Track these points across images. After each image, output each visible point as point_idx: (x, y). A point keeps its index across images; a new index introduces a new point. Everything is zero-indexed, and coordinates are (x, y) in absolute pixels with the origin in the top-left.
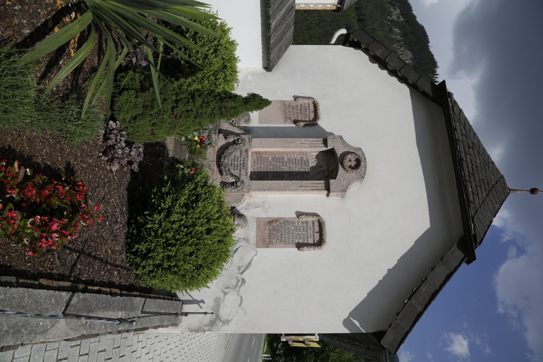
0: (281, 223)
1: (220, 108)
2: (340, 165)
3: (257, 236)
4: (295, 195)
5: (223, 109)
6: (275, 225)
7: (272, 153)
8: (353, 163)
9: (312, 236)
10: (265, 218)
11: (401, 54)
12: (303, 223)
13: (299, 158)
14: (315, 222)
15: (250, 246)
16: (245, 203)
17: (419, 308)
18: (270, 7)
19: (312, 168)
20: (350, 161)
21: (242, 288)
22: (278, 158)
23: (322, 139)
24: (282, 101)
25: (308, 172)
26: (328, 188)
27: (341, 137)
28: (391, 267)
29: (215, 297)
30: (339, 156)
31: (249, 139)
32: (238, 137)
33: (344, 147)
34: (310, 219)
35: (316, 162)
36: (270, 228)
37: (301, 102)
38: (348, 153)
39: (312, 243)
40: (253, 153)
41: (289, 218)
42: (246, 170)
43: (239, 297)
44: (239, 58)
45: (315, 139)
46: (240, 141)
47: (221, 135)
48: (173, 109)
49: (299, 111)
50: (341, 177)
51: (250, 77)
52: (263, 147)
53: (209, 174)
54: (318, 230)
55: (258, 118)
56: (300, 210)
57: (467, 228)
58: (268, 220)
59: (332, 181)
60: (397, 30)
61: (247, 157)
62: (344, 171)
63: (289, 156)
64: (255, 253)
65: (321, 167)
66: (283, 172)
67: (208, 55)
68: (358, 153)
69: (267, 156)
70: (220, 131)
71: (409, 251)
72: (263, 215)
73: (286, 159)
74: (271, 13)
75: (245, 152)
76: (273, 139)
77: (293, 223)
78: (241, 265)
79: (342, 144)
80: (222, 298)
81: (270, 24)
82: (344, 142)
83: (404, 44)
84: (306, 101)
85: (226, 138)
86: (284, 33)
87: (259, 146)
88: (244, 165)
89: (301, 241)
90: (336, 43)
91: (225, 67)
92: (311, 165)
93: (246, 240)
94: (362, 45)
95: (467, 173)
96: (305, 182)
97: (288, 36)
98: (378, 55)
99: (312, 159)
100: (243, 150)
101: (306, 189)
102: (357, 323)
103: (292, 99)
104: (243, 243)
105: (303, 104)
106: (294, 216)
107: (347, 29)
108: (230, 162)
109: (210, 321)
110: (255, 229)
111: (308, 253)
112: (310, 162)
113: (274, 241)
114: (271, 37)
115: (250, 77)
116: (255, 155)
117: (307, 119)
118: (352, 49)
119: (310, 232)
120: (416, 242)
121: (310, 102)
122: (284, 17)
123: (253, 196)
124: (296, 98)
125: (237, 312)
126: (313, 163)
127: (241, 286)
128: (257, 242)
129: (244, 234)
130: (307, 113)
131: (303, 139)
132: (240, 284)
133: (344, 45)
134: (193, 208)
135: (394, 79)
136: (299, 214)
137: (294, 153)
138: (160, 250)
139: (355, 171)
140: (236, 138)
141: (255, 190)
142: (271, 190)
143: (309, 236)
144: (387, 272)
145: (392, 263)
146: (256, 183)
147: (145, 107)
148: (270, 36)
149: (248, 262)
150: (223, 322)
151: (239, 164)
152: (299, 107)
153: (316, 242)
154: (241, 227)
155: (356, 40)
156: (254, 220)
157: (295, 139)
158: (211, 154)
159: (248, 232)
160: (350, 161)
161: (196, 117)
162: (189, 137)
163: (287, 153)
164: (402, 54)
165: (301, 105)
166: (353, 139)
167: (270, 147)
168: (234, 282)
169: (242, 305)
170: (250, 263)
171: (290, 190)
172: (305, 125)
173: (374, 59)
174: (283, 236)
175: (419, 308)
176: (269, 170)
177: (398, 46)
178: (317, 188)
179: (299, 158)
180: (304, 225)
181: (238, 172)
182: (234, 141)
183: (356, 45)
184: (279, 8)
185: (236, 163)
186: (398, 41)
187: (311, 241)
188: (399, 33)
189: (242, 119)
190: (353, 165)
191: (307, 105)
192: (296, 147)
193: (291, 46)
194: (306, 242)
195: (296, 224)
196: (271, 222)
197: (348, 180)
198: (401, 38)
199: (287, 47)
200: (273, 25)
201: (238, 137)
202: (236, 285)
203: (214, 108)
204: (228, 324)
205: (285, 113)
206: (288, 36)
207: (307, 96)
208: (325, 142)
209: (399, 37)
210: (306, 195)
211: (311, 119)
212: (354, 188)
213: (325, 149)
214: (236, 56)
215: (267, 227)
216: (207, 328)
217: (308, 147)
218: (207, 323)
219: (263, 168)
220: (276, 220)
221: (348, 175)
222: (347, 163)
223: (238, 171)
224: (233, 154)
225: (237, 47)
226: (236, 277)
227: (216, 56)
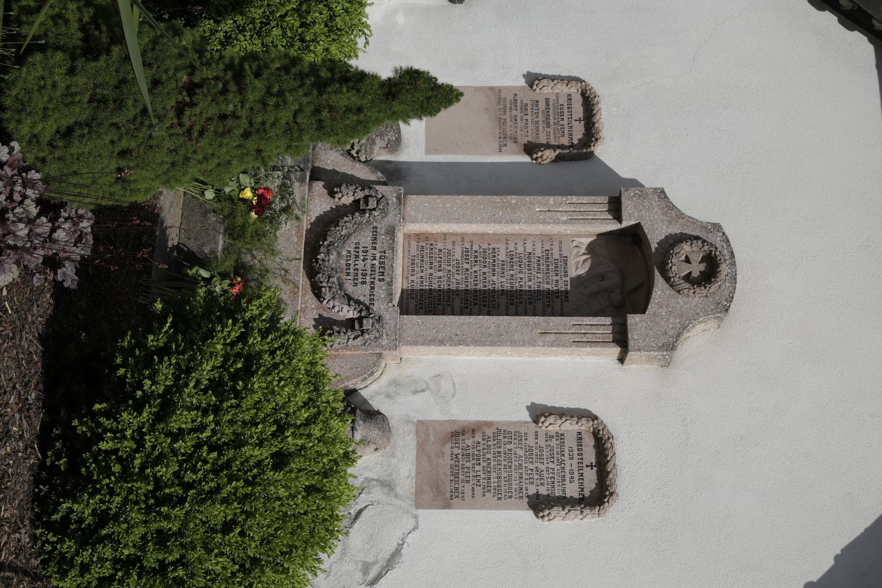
0: (485, 438)
2: (657, 274)
3: (418, 473)
4: (526, 359)
5: (325, 113)
6: (469, 442)
7: (463, 237)
8: (697, 269)
9: (576, 476)
12: (549, 437)
13: (538, 253)
14: (573, 97)
15: (398, 502)
16: (384, 380)
19: (577, 281)
20: (687, 260)
22: (479, 253)
23: (605, 199)
24: (491, 88)
25: (566, 292)
26: (621, 339)
27: (663, 191)
30: (654, 246)
31: (399, 198)
33: (670, 222)
34: (570, 427)
35: (588, 264)
36: (456, 451)
38: (682, 238)
40: (408, 237)
41: (511, 423)
42: (390, 284)
45: (585, 199)
46: (372, 203)
47: (319, 186)
48: (180, 111)
49: (541, 118)
51: (400, 19)
52: (438, 222)
53: (285, 297)
54: (593, 460)
55: (424, 137)
59: (633, 320)
61: (393, 249)
62: (669, 291)
63: (511, 247)
64: (411, 523)
65: (602, 277)
66: (494, 291)
68: (711, 238)
69: (450, 247)
70: (317, 174)
72: (436, 415)
73: (502, 256)
75: (387, 233)
76: (467, 198)
77: (520, 437)
78: (370, 559)
79: (665, 214)
82: (671, 207)
84: (562, 89)
85: (332, 194)
87: (426, 219)
88: (383, 271)
89: (543, 491)
92: (573, 273)
93: (388, 485)
96: (555, 322)
99: (577, 255)
100: (382, 228)
101: (558, 341)
103: (522, 82)
104: (377, 494)
105: (552, 98)
106: (526, 417)
108: (343, 262)
110: (414, 453)
111: (565, 526)
112: (571, 262)
113: (468, 488)
115: (400, 19)
116: (414, 244)
117: (565, 141)
119: (571, 465)
124: (533, 80)
126: (579, 266)
128: (419, 492)
129: (380, 466)
130: (565, 122)
131: (551, 200)
135: (829, 19)
136: (539, 413)
137: (525, 238)
138: (136, 516)
139: (701, 291)
140: (360, 195)
141: (415, 343)
143: (568, 476)
149: (392, 549)
151: (368, 267)
152: (542, 105)
153: (587, 493)
154: (373, 447)
156: (411, 427)
157: (528, 199)
158: (290, 238)
159: (394, 461)
160: (687, 260)
161: (246, 135)
163: (507, 238)
165: (547, 100)
167: (458, 220)
170: (396, 554)
171: (513, 343)
172: (558, 159)
176: (453, 287)
178: (590, 338)
179: (538, 253)
180: (554, 443)
181: (367, 292)
182: (357, 202)
185: (360, 264)
187: (572, 491)
190: (696, 274)
191: (563, 100)
192: (531, 221)
194: (558, 493)
195: (531, 441)
196: (459, 433)
197: (681, 316)
201: (367, 192)
205: (501, 122)
207: (564, 74)
208: (615, 208)
211: (575, 141)
212: (699, 340)
213: (614, 226)
219: (437, 279)
220: (472, 429)
222: (678, 268)
223: (367, 288)
224: (353, 240)
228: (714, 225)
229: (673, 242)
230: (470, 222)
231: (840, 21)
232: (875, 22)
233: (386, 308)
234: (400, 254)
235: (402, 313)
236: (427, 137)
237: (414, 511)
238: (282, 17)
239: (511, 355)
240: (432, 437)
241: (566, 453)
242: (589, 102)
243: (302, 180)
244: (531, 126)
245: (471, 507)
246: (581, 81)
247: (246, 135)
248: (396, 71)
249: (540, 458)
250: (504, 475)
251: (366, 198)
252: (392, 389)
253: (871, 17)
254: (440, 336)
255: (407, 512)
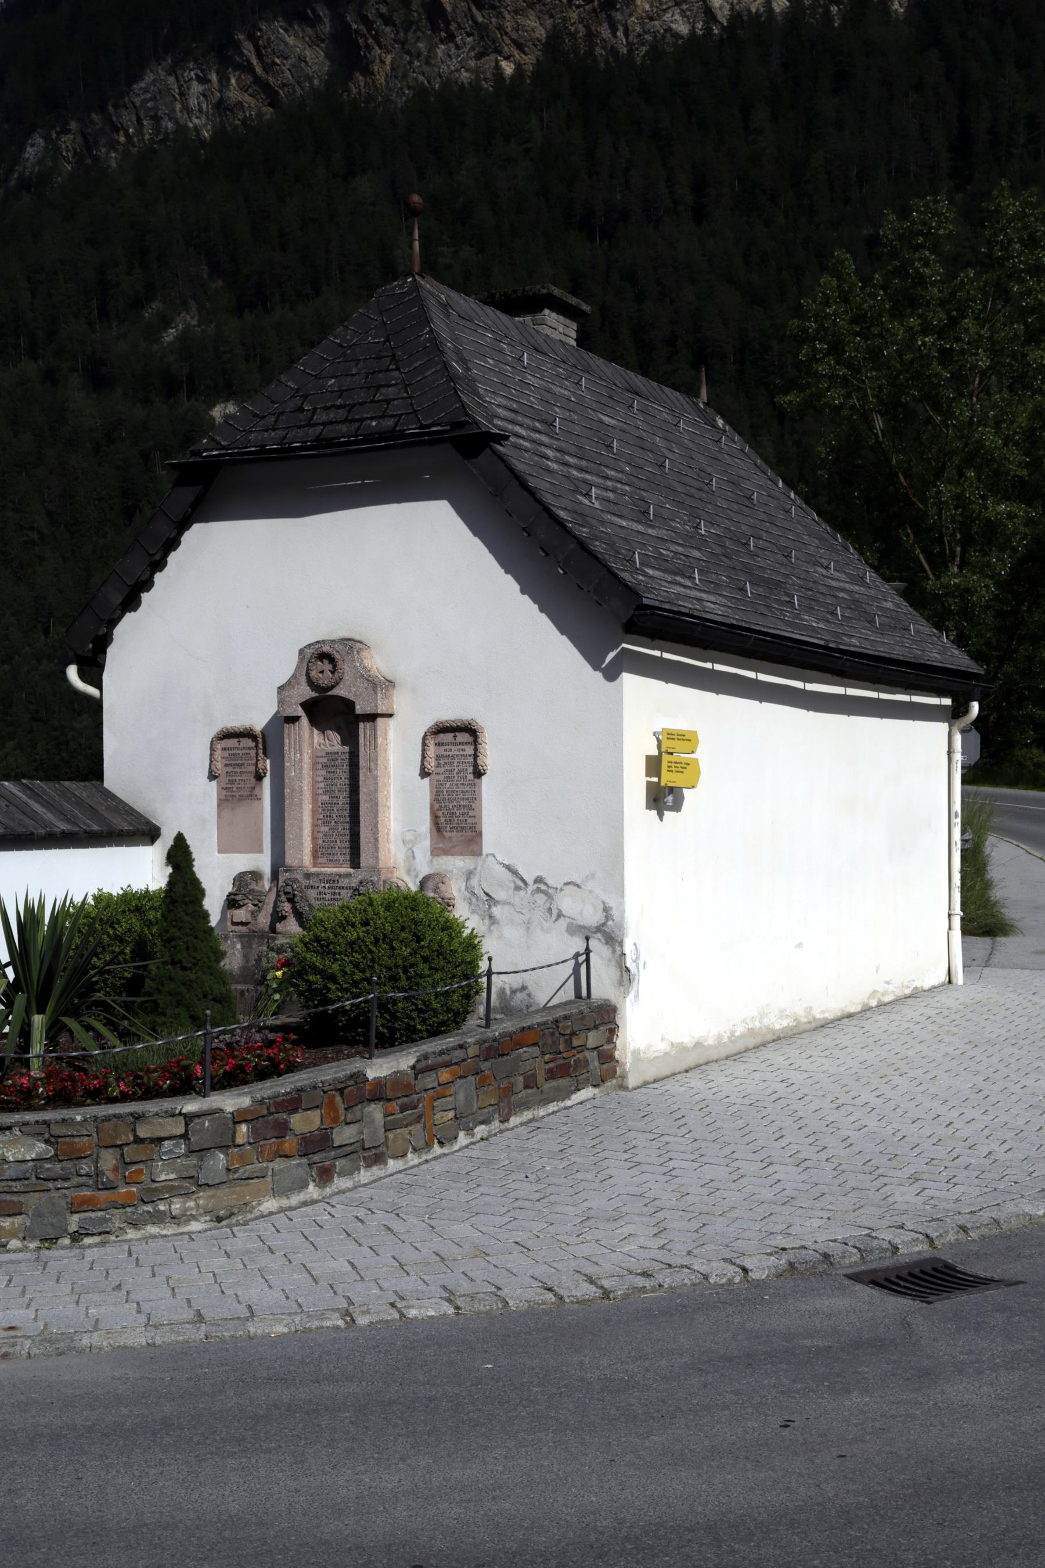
1: (185, 903)
2: (330, 693)
3: (462, 854)
4: (392, 780)
5: (186, 899)
6: (443, 820)
7: (314, 825)
8: (327, 666)
9: (461, 747)
10: (432, 839)
11: (157, 129)
12: (438, 765)
13: (324, 772)
15: (479, 868)
17: (572, 546)
18: (32, 834)
20: (322, 672)
21: (550, 882)
22: (323, 815)
23: (286, 726)
24: (219, 806)
26: (372, 717)
27: (279, 688)
28: (517, 587)
29: (566, 935)
31: (286, 871)
32: (282, 893)
33: (299, 684)
34: (432, 751)
35: (330, 732)
37: (219, 765)
38: (308, 675)
39: (473, 747)
40: (315, 865)
41: (431, 792)
42: (340, 876)
43: (566, 887)
44: (125, 887)
45: (286, 741)
46: (289, 889)
47: (279, 926)
48: (184, 969)
49: (238, 770)
50: (350, 692)
52: (302, 844)
55: (251, 855)
56: (418, 771)
57: (436, 440)
58: (435, 833)
59: (359, 709)
60: (31, 153)
62: (341, 685)
63: (320, 791)
64: (491, 858)
67: (117, 936)
68: (308, 656)
69: (321, 835)
70: (273, 929)
71: (492, 551)
72: (427, 843)
73: (326, 798)
74: (42, 831)
75: (308, 879)
76: (287, 824)
78: (512, 886)
79: (293, 687)
80: (568, 920)
81: (63, 832)
82: (289, 682)
83: (102, 109)
84: (218, 754)
85: (284, 918)
86: (79, 802)
87: (302, 853)
88: (332, 880)
89: (471, 769)
90: (99, 686)
91: (138, 909)
93: (469, 875)
94: (101, 633)
95: (344, 428)
97: (85, 794)
98: (119, 601)
99: (325, 745)
100: (305, 882)
102: (611, 655)
103: (214, 783)
104: (474, 882)
107: (71, 663)
109: (607, 943)
111: (491, 756)
112: (329, 749)
113: (470, 820)
114: (88, 829)
116: (320, 860)
117: (253, 753)
118: (111, 651)
120: (475, 535)
121: (219, 746)
122: (48, 805)
123: (395, 863)
124: (212, 777)
125: (591, 892)
126: (334, 742)
127: (546, 884)
130: (240, 752)
131: (287, 764)
132: (543, 887)
133: (101, 667)
134: (328, 945)
135: (173, 558)
137: (314, 782)
139: (340, 664)
140: (283, 898)
141: (377, 858)
142: (376, 827)
143: (462, 753)
144: (526, 596)
145: (509, 584)
146: (365, 859)
147: (179, 1003)
148: (86, 832)
149: (506, 871)
150: (607, 918)
152: (230, 769)
154: (440, 885)
155: (91, 646)
156: (435, 859)
159: (455, 871)
160: (323, 674)
161: (196, 937)
162: (275, 986)
163: (315, 795)
164: (156, 119)
165: (226, 765)
166: (286, 666)
167: (301, 829)
168: (541, 898)
169: (579, 882)
170: (509, 868)
171: (376, 791)
173: (131, 603)
174: (462, 803)
175: (572, 546)
177: (113, 145)
179: (324, 772)
180: (442, 762)
181: (345, 891)
183: (103, 642)
184: (34, 816)
185: (328, 896)
186: (89, 144)
187: (469, 750)
188: (47, 139)
189: (251, 887)
190: (330, 667)
191: (226, 754)
192: (300, 777)
193: (110, 782)
196: (437, 827)
198: (73, 125)
199: (109, 795)
200: (63, 826)
201: (282, 893)
202: (546, 893)
203: (184, 911)
204: (611, 908)
205: (241, 799)
206: (85, 794)
207: (209, 752)
208: (293, 720)
209: (66, 140)
210: (391, 758)
212: (377, 663)
213: (305, 721)
214: (121, 892)
215: (447, 835)
216: (618, 948)
217: (301, 755)
218: (610, 950)
219: (343, 843)
221: (347, 678)
222: (325, 679)
223: (343, 892)
224: (313, 902)
225: (105, 891)
226: (532, 894)
227: (119, 923)
228: (300, 654)
229: (311, 683)
230: (302, 821)
231: (175, 550)
232: (172, 536)
233: (359, 875)
234: (323, 870)
235: (359, 867)
236: (246, 852)
237: (484, 856)
238: (152, 935)
239: (388, 792)
240: (441, 845)
241: (447, 753)
242: (227, 735)
243: (274, 939)
244: (244, 777)
245: (481, 818)
246: (212, 741)
247: (196, 937)
248: (167, 865)
249: (451, 771)
250: (461, 796)
251: (286, 893)
252: (413, 874)
253: (168, 539)
254: (372, 840)
255: (484, 861)
